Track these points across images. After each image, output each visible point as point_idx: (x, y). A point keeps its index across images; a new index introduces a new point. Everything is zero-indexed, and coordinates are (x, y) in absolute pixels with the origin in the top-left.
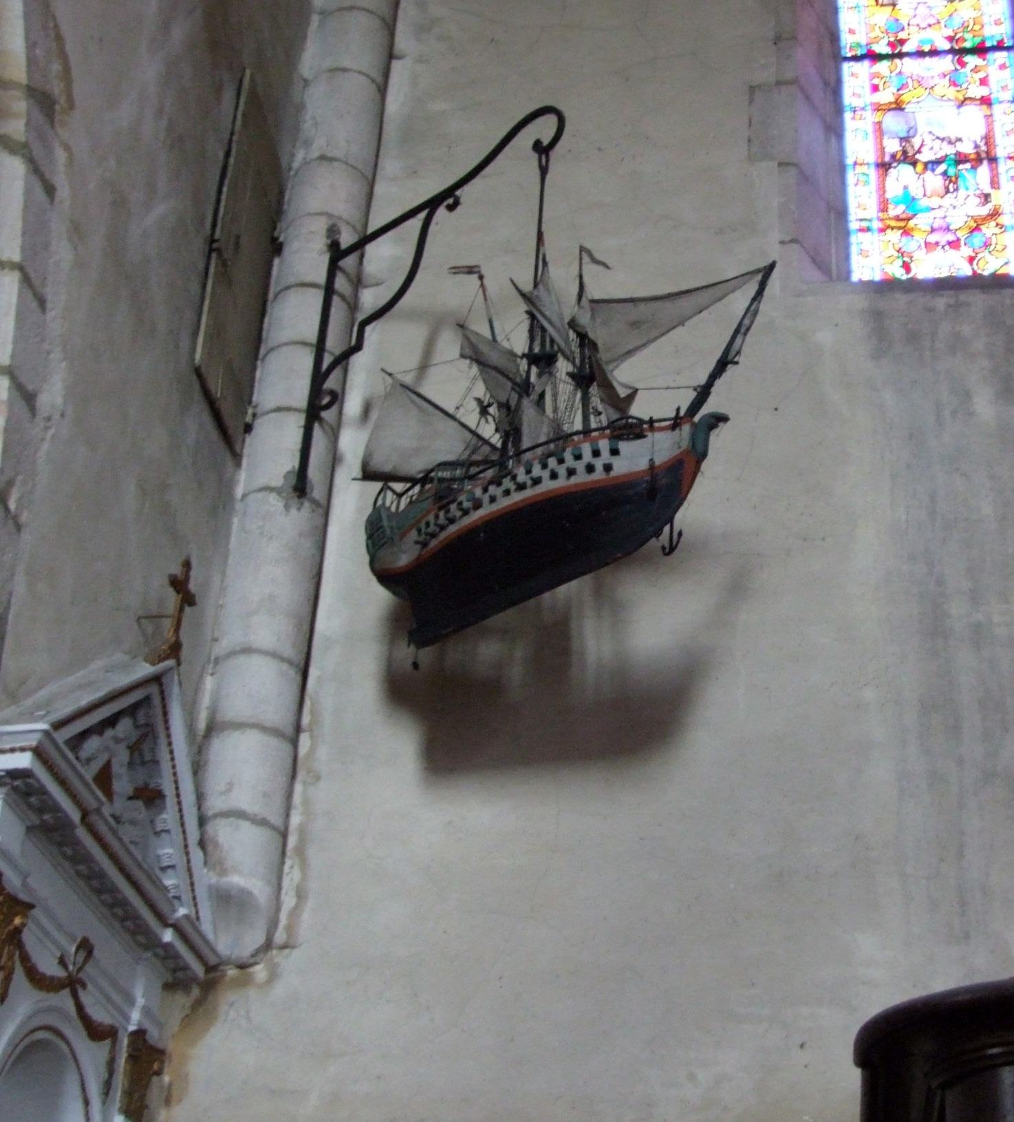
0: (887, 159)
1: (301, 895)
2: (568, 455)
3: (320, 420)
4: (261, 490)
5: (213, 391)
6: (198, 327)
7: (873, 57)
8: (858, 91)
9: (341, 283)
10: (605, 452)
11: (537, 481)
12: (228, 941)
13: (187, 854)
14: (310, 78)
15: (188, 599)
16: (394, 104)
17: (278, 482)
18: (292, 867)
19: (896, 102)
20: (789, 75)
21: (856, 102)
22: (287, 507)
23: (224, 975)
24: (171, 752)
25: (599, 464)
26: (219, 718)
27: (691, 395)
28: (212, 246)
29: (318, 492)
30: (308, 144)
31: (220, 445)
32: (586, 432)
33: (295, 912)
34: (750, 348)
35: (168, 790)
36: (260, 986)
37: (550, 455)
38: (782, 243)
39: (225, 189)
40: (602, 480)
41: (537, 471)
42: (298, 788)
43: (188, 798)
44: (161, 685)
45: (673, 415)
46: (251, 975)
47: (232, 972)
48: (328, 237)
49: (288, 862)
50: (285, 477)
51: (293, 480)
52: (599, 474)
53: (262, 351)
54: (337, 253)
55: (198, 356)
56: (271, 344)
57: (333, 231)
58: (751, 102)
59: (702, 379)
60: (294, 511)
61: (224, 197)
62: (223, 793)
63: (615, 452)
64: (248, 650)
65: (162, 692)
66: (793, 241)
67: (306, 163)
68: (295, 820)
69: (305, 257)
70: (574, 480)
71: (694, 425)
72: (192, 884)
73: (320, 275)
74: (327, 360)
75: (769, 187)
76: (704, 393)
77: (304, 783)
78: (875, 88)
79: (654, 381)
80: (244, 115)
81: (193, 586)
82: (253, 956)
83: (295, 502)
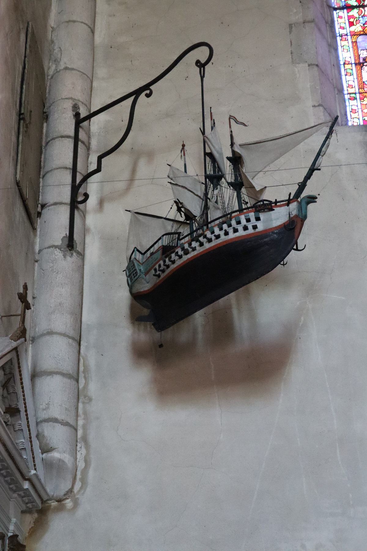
0: (361, 61)
1: (87, 461)
2: (233, 222)
3: (78, 208)
4: (49, 247)
5: (25, 193)
6: (17, 161)
7: (349, 8)
8: (343, 25)
9: (82, 135)
10: (253, 219)
11: (218, 237)
12: (54, 487)
13: (31, 442)
14: (55, 26)
15: (27, 306)
16: (98, 39)
17: (59, 243)
18: (81, 448)
19: (363, 31)
20: (310, 18)
21: (343, 32)
22: (65, 256)
23: (50, 506)
24: (23, 388)
25: (250, 226)
26: (38, 369)
27: (297, 187)
28: (21, 117)
29: (79, 248)
30: (57, 62)
31: (27, 224)
32: (241, 210)
33: (85, 471)
34: (323, 161)
35: (22, 409)
36: (69, 510)
37: (224, 223)
38: (314, 106)
39: (24, 86)
40: (253, 233)
41: (217, 231)
42: (81, 405)
43: (30, 412)
44: (17, 352)
45: (287, 198)
46: (64, 505)
47: (54, 504)
48: (73, 111)
49: (79, 445)
50: (62, 240)
51: (66, 242)
52: (251, 231)
53: (272, 167)
54: (79, 121)
55: (18, 176)
56: (47, 169)
57: (75, 107)
58: (290, 32)
59: (301, 180)
60: (68, 258)
61: (24, 91)
62: (44, 410)
63: (258, 219)
64: (50, 333)
65: (18, 356)
66: (319, 105)
67: (57, 72)
68: (81, 422)
69: (63, 122)
70: (237, 234)
71: (300, 203)
72: (34, 458)
73: (71, 132)
74: (79, 178)
75: (305, 78)
76: (302, 186)
77: (83, 403)
78: (351, 24)
79: (274, 180)
80: (30, 47)
81: (29, 299)
82: (65, 495)
83: (68, 253)
